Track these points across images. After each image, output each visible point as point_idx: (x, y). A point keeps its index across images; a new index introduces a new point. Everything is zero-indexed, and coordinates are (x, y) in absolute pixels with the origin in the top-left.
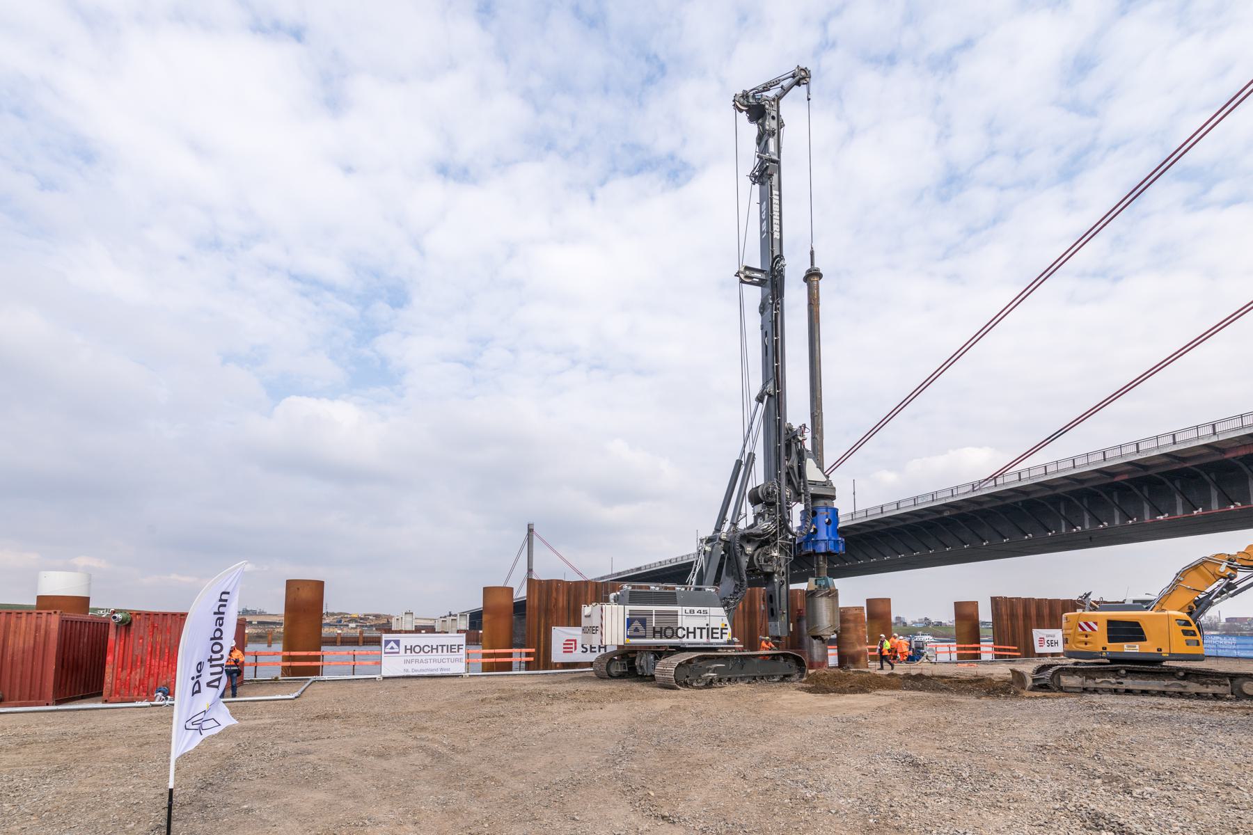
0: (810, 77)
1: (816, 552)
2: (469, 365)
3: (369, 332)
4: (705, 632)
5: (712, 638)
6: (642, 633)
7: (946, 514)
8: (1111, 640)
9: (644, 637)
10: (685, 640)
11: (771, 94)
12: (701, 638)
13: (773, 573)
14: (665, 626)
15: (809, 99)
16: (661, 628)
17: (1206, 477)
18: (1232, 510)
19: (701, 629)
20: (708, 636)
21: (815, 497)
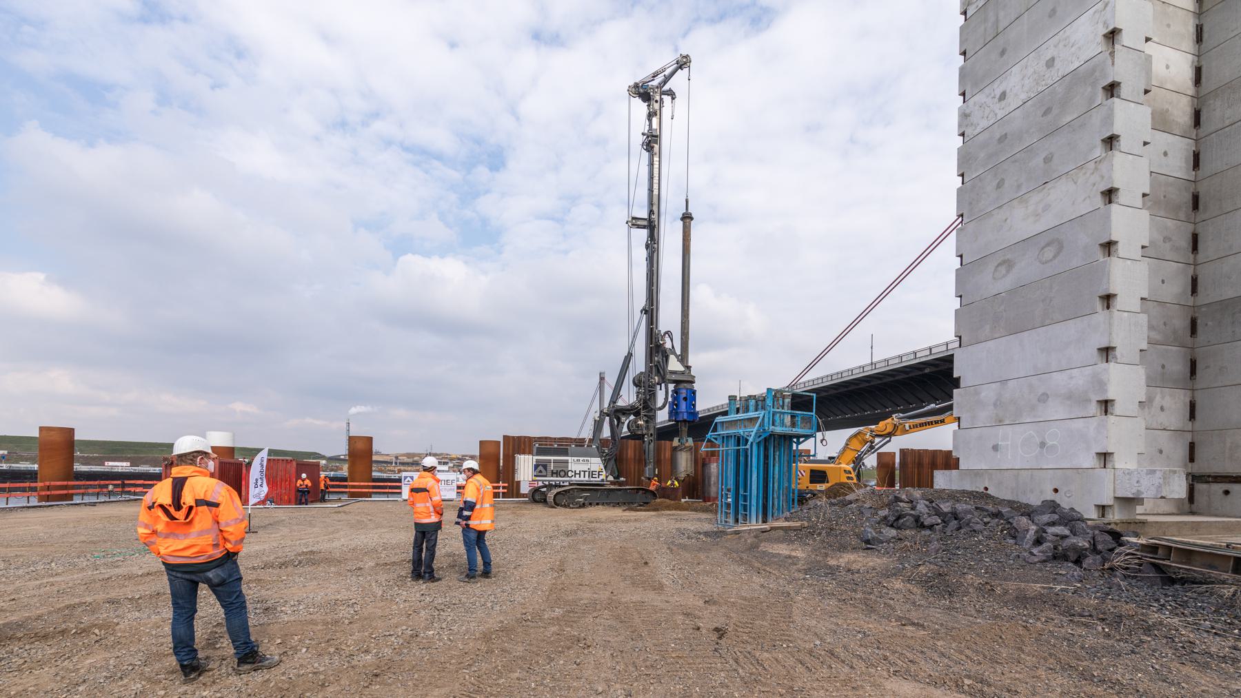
2: (560, 221)
3: (470, 195)
4: (587, 473)
5: (592, 477)
6: (544, 473)
7: (927, 371)
8: (811, 482)
9: (546, 476)
10: (573, 478)
12: (584, 477)
13: (643, 435)
15: (689, 80)
19: (585, 472)
21: (677, 382)
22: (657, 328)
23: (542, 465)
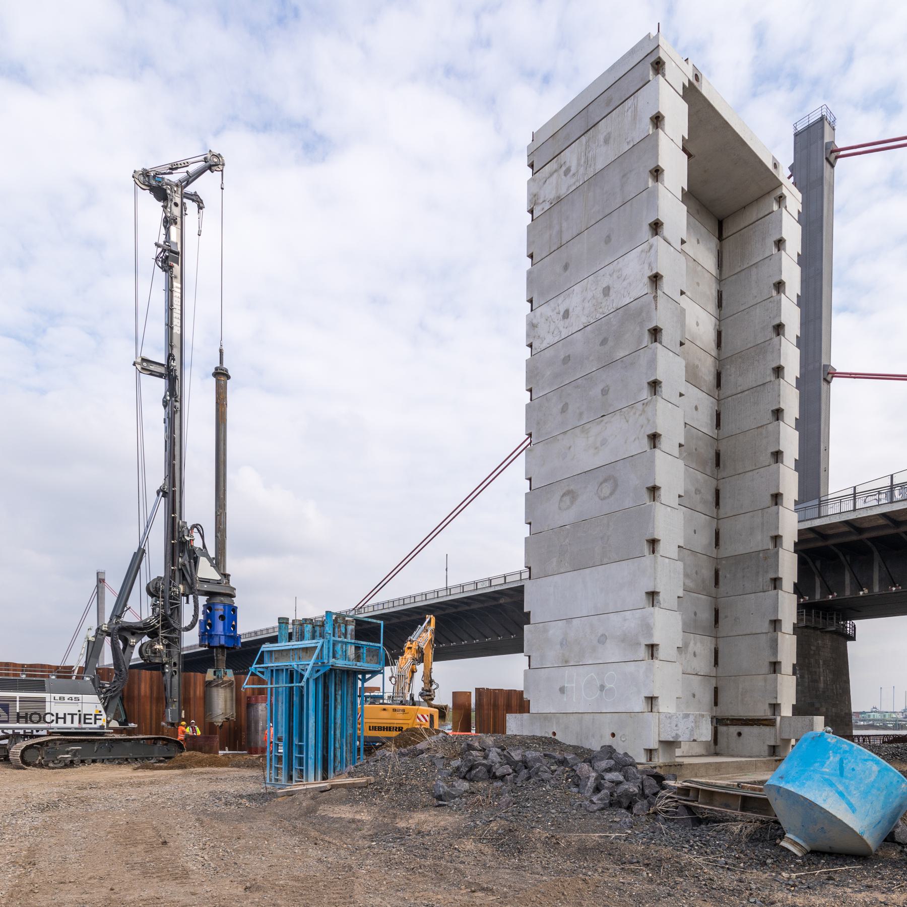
0: (223, 165)
1: (211, 645)
4: (76, 718)
5: (85, 723)
6: (5, 718)
9: (7, 722)
10: (54, 725)
11: (175, 177)
12: (72, 722)
13: (163, 665)
14: (30, 711)
16: (27, 714)
17: (842, 558)
18: (830, 600)
19: (72, 715)
20: (80, 722)
21: (211, 594)
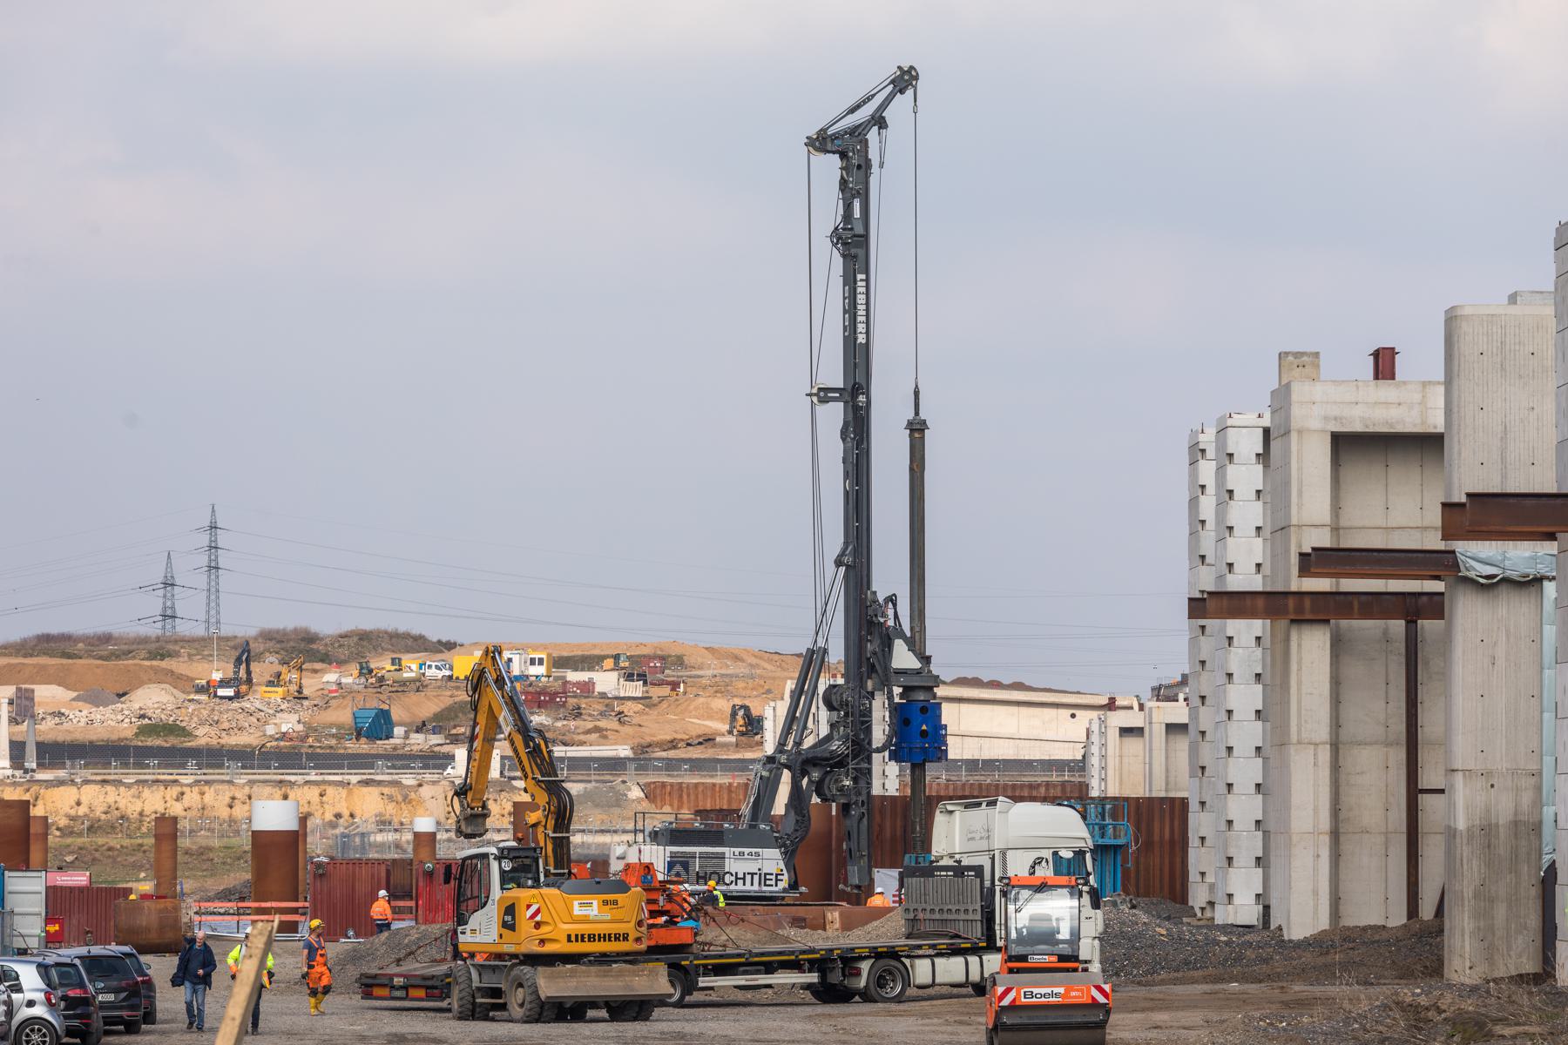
4: (756, 878)
5: (765, 885)
10: (733, 887)
12: (752, 884)
19: (752, 874)
22: (869, 588)
23: (681, 863)
